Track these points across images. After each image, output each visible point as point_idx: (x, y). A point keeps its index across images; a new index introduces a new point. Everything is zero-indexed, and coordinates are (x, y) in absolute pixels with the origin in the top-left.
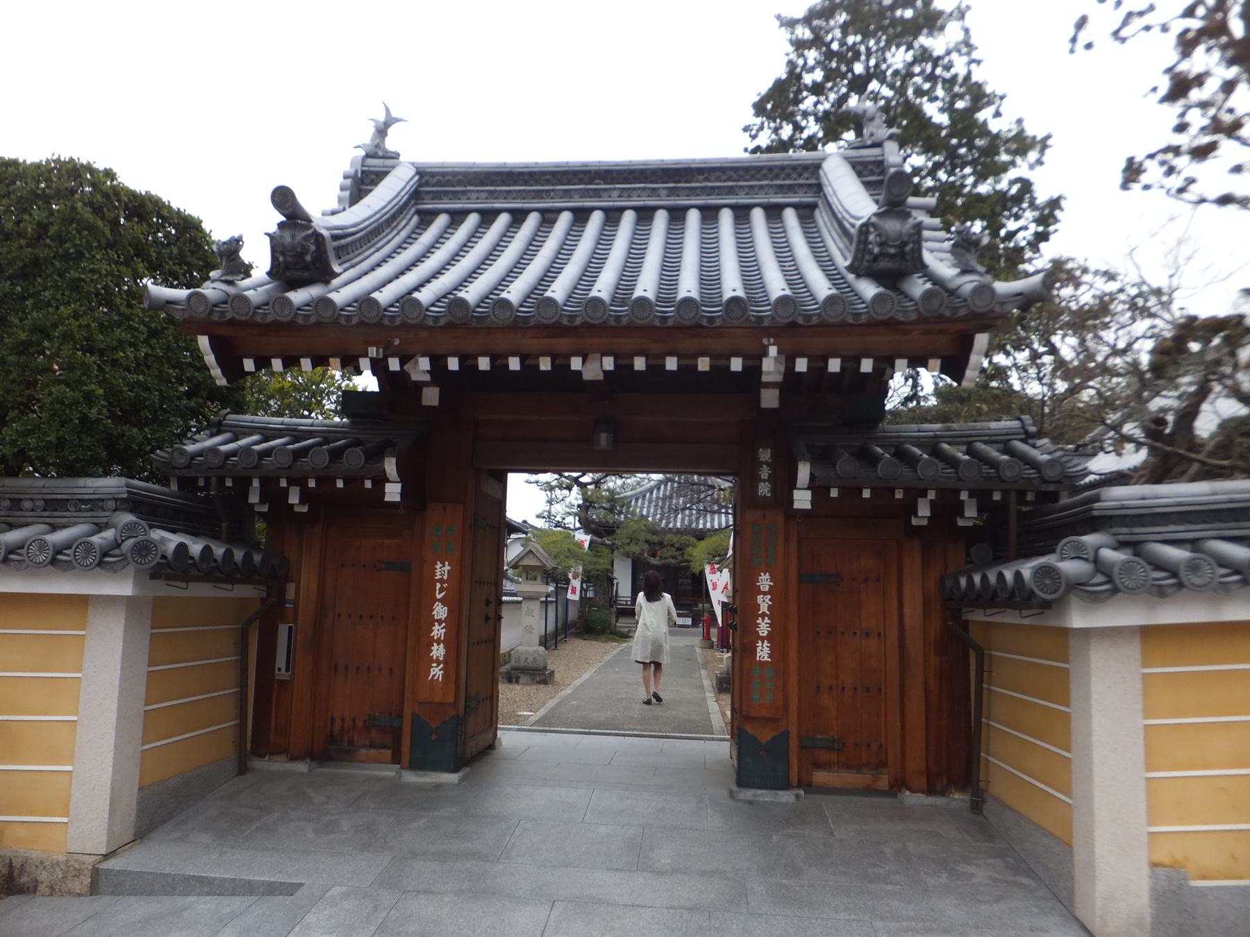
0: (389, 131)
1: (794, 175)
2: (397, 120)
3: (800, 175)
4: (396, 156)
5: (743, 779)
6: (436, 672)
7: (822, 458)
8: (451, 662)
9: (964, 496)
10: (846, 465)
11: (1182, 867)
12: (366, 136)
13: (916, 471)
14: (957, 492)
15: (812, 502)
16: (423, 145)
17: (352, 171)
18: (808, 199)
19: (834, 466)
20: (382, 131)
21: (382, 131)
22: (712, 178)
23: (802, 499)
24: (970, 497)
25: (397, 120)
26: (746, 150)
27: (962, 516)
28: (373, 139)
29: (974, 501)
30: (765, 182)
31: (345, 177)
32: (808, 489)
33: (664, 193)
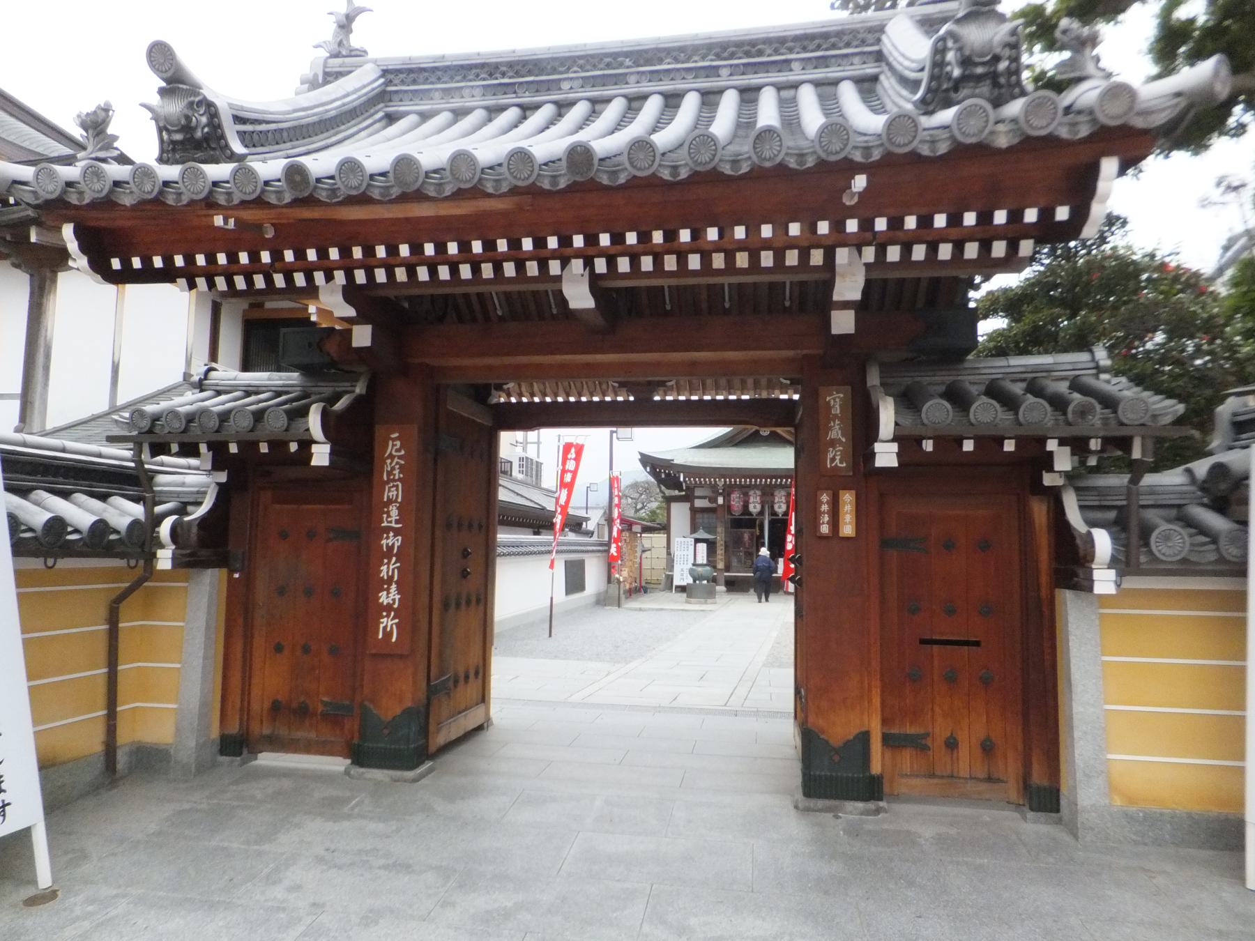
0: (354, 26)
1: (588, 67)
2: (361, 10)
3: (569, 69)
4: (362, 53)
5: (832, 773)
6: (388, 623)
7: (909, 401)
8: (405, 613)
9: (1052, 445)
10: (937, 411)
11: (823, 732)
12: (328, 31)
13: (1017, 414)
14: (1042, 441)
15: (899, 455)
16: (388, 40)
17: (311, 76)
18: (870, 70)
19: (919, 411)
20: (346, 25)
21: (346, 25)
22: (524, 71)
23: (886, 455)
24: (1060, 444)
25: (361, 10)
26: (832, 6)
27: (1050, 469)
28: (335, 36)
29: (1067, 449)
30: (531, 78)
31: (302, 83)
32: (893, 440)
33: (477, 92)
